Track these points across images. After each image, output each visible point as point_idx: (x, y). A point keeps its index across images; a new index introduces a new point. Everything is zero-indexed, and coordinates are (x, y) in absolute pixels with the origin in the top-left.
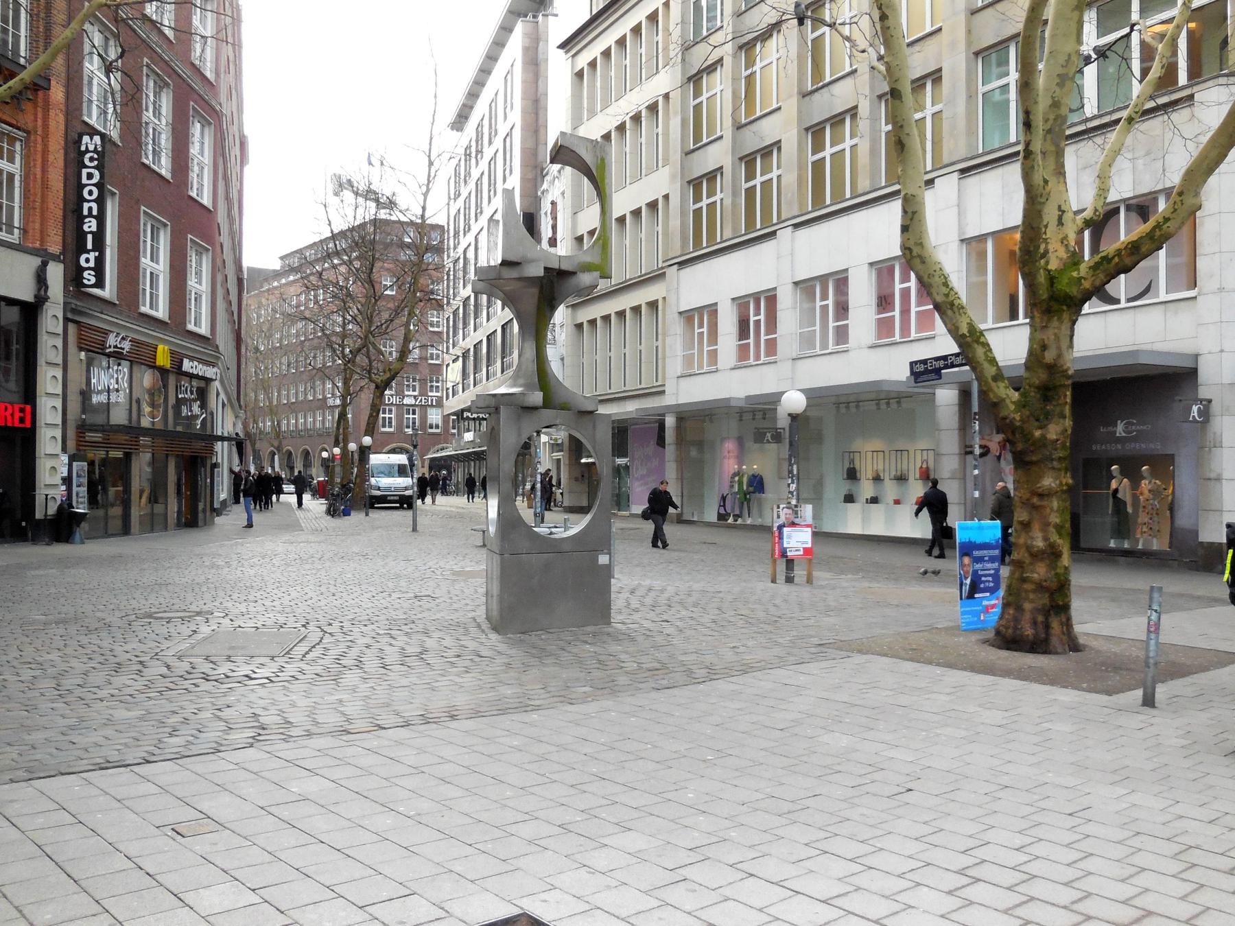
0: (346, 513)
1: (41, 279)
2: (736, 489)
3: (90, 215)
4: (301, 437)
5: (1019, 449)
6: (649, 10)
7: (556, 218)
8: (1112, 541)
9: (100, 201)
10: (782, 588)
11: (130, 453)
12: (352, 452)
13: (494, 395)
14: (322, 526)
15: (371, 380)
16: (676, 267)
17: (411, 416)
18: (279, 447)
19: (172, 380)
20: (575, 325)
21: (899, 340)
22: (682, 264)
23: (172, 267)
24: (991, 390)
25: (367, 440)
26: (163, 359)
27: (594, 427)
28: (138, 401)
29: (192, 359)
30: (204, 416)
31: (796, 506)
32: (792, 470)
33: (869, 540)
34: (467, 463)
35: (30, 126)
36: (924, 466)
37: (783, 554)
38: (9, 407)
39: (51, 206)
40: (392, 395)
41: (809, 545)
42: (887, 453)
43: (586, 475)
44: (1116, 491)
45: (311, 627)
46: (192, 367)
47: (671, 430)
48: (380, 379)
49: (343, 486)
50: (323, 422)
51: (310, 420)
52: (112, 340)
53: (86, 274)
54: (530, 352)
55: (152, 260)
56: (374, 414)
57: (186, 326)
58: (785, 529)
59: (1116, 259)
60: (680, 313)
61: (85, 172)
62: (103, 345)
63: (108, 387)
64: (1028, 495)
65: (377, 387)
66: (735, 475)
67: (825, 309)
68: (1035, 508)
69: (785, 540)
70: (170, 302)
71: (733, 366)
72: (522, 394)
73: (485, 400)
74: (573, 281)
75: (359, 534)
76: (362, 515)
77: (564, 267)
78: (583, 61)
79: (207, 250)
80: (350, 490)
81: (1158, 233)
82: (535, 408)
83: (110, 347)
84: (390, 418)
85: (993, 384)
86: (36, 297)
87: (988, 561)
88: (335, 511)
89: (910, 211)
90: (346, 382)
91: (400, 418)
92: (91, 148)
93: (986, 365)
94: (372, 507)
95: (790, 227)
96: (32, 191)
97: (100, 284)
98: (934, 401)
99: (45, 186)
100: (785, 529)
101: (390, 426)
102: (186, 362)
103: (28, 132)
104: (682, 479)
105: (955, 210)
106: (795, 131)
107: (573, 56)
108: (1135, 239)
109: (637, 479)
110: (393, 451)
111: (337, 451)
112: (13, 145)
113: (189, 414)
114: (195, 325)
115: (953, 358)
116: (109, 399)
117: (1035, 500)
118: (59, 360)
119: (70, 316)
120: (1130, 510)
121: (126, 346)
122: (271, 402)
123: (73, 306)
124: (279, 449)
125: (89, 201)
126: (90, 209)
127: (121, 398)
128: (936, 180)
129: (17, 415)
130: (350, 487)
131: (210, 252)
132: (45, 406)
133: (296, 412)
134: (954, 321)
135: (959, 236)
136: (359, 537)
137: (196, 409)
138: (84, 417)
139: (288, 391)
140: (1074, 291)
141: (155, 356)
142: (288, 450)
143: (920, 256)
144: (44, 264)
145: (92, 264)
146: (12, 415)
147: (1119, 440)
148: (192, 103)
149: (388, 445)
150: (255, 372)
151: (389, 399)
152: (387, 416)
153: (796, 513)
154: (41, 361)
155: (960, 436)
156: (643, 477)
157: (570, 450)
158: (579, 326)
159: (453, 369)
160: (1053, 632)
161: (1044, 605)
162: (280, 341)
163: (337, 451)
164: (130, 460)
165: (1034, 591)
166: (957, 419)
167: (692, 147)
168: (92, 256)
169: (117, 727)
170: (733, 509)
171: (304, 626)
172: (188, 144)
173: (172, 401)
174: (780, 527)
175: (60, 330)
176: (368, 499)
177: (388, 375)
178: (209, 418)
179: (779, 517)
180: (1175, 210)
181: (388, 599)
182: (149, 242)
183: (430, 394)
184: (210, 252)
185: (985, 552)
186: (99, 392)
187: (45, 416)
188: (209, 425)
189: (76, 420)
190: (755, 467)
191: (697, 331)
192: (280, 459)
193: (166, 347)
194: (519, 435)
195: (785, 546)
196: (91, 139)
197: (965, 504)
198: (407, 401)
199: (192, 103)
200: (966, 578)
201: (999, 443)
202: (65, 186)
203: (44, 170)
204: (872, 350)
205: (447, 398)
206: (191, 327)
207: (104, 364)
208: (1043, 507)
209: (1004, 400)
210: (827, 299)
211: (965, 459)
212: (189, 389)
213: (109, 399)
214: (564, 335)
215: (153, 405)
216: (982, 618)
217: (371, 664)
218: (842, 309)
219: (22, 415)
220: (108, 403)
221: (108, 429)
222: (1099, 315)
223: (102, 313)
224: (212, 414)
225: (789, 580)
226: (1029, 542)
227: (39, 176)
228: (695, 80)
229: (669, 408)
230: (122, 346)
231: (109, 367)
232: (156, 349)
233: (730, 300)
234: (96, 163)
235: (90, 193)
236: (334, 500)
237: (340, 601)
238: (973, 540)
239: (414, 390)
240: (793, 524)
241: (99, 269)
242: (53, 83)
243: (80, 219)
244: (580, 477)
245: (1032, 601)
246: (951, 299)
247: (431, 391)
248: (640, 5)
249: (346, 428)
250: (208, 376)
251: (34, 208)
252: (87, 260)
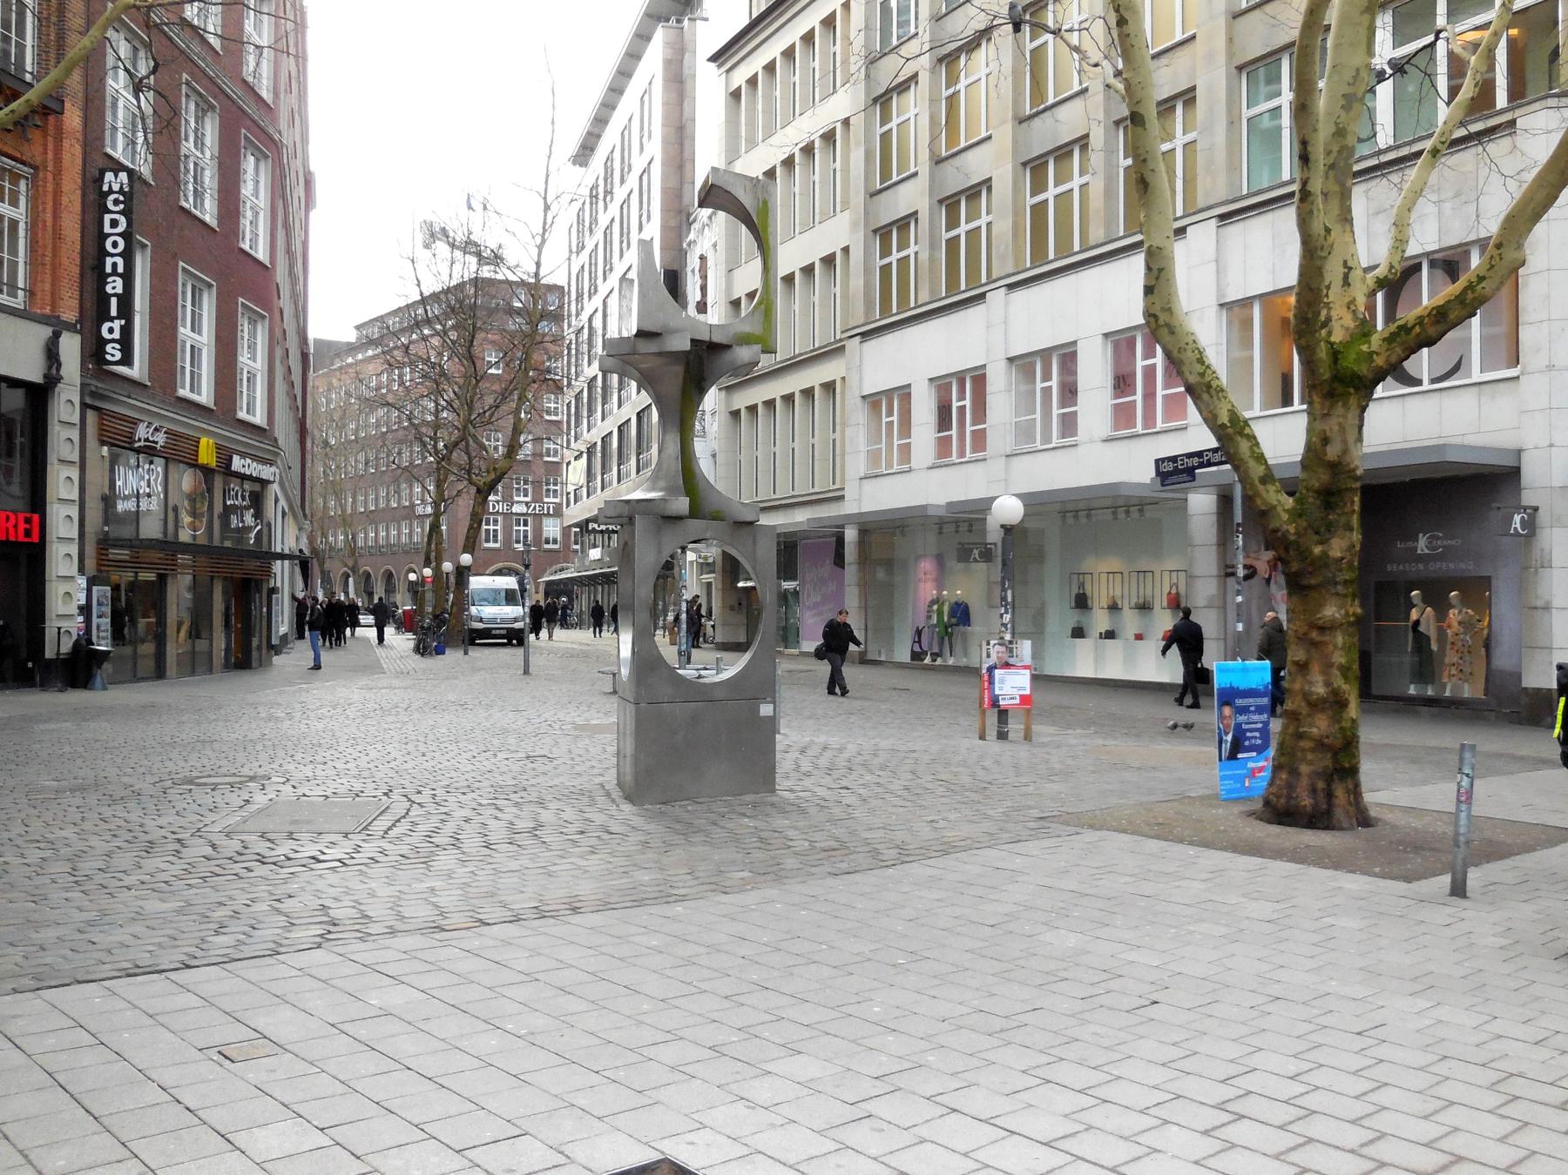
0: (440, 651)
1: (52, 354)
2: (934, 620)
3: (114, 273)
4: (383, 554)
5: (1293, 570)
6: (825, 13)
7: (706, 277)
8: (1412, 686)
9: (128, 255)
10: (993, 746)
11: (165, 575)
12: (447, 574)
13: (628, 502)
14: (409, 667)
15: (471, 482)
16: (858, 339)
17: (522, 528)
18: (354, 567)
19: (218, 482)
20: (730, 413)
21: (1141, 432)
22: (865, 335)
23: (218, 338)
24: (1258, 494)
25: (466, 559)
26: (207, 456)
27: (754, 542)
28: (175, 509)
29: (243, 455)
30: (259, 527)
31: (1011, 642)
32: (1006, 597)
33: (1103, 685)
34: (592, 588)
35: (38, 160)
36: (1174, 591)
37: (995, 702)
38: (12, 516)
39: (65, 261)
40: (498, 502)
41: (1028, 692)
42: (1126, 575)
43: (744, 603)
44: (1417, 623)
45: (395, 796)
46: (244, 466)
47: (852, 546)
48: (483, 480)
49: (436, 617)
50: (410, 535)
51: (394, 533)
52: (142, 432)
53: (109, 348)
54: (673, 447)
55: (193, 330)
56: (475, 526)
57: (236, 414)
58: (997, 672)
59: (1417, 329)
60: (864, 397)
61: (107, 218)
62: (131, 438)
63: (138, 491)
64: (1305, 629)
65: (479, 491)
66: (933, 602)
67: (1047, 392)
68: (1315, 644)
69: (997, 685)
70: (216, 383)
71: (930, 464)
72: (663, 500)
73: (615, 507)
74: (727, 357)
75: (456, 678)
76: (459, 654)
77: (717, 339)
78: (740, 77)
79: (263, 317)
80: (444, 622)
81: (1470, 296)
82: (679, 518)
83: (140, 440)
84: (495, 531)
85: (1261, 487)
86: (45, 376)
87: (1254, 712)
88: (425, 648)
89: (1155, 267)
90: (439, 485)
91: (507, 530)
92: (116, 187)
93: (1252, 463)
94: (473, 643)
95: (1003, 289)
96: (40, 243)
97: (127, 360)
98: (1186, 508)
99: (57, 235)
100: (997, 672)
101: (496, 541)
102: (236, 459)
103: (35, 168)
104: (866, 608)
105: (1213, 266)
106: (1010, 166)
107: (728, 71)
108: (1441, 303)
109: (809, 608)
110: (499, 573)
111: (428, 572)
112: (17, 184)
113: (240, 525)
114: (248, 412)
115: (1210, 454)
116: (138, 506)
117: (1314, 635)
118: (75, 457)
119: (88, 400)
120: (1434, 647)
121: (161, 439)
122: (344, 511)
123: (93, 389)
124: (354, 569)
125: (113, 255)
126: (115, 265)
127: (153, 505)
128: (1188, 229)
129: (22, 526)
130: (445, 618)
131: (267, 320)
132: (57, 515)
133: (376, 523)
134: (1212, 407)
135: (1218, 300)
136: (455, 681)
137: (249, 518)
138: (106, 529)
139: (366, 496)
140: (1364, 370)
141: (197, 451)
142: (365, 571)
143: (1167, 325)
144: (56, 335)
145: (116, 335)
146: (15, 526)
147: (1421, 558)
148: (243, 131)
149: (493, 565)
150: (324, 472)
151: (494, 507)
152: (491, 527)
153: (1011, 651)
154: (52, 458)
155: (1219, 553)
156: (816, 605)
157: (724, 571)
158: (735, 414)
159: (575, 468)
160: (1337, 801)
161: (1326, 767)
162: (356, 432)
163: (428, 572)
164: (166, 584)
165: (1313, 750)
166: (1215, 532)
167: (878, 187)
168: (117, 325)
169: (148, 923)
170: (931, 646)
171: (385, 794)
173: (218, 508)
174: (991, 669)
175: (76, 419)
176: (467, 633)
177: (493, 476)
178: (265, 531)
179: (988, 656)
180: (1492, 267)
181: (493, 760)
182: (189, 308)
183: (546, 500)
184: (267, 320)
185: (1251, 700)
186: (126, 498)
187: (57, 528)
188: (265, 539)
189: (96, 533)
190: (959, 592)
191: (885, 420)
192: (356, 583)
193: (211, 441)
194: (660, 552)
195: (997, 693)
196: (116, 177)
197: (1225, 639)
198: (516, 509)
199: (243, 131)
200: (1227, 734)
201: (1269, 562)
202: (83, 236)
203: (56, 216)
204: (1107, 444)
205: (568, 505)
206: (242, 415)
207: (133, 461)
208: (1324, 643)
209: (1274, 507)
210: (1050, 379)
211: (1225, 583)
212: (239, 494)
213: (138, 506)
214: (716, 425)
215: (194, 514)
216: (1247, 784)
217: (471, 843)
218: (1070, 392)
219: (28, 526)
220: (138, 512)
221: (137, 545)
222: (1395, 400)
223: (129, 397)
224: (269, 525)
225: (1002, 736)
226: (1307, 688)
227: (49, 223)
228: (882, 101)
229: (849, 518)
230: (155, 439)
231: (138, 466)
232: (198, 442)
233: (927, 381)
234: (122, 206)
235: (115, 245)
236: (424, 634)
237: (431, 763)
238: (1235, 685)
239: (526, 495)
240: (1007, 665)
241: (126, 342)
242: (67, 105)
243: (102, 278)
244: (737, 605)
245: (1310, 763)
246: (1208, 379)
247: (548, 496)
248: (812, 6)
249: (439, 543)
250: (264, 478)
251: (44, 265)
252: (111, 330)
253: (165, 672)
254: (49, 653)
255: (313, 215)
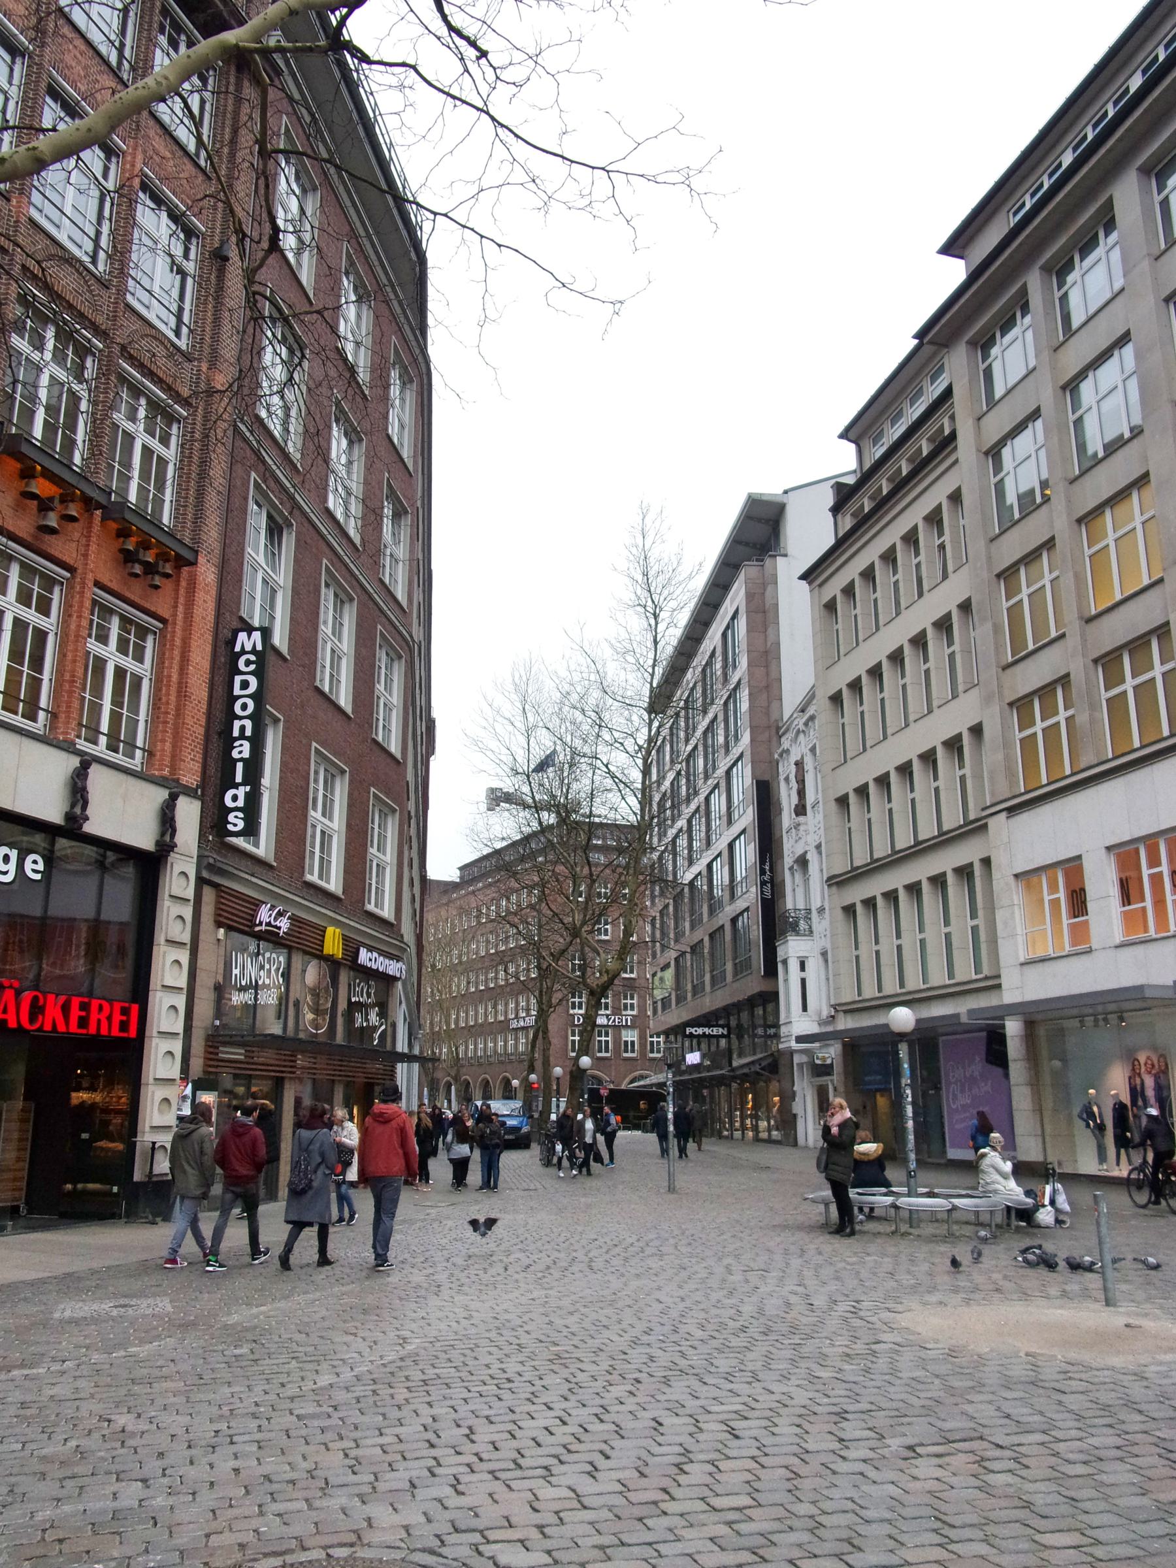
1: (167, 820)
3: (242, 736)
4: (480, 1065)
7: (803, 781)
9: (256, 717)
11: (283, 1079)
12: (558, 1079)
16: (1004, 815)
19: (344, 977)
21: (1154, 936)
22: (1012, 811)
23: (349, 826)
26: (333, 944)
28: (297, 1004)
29: (371, 949)
30: (383, 1027)
35: (166, 614)
38: (106, 1005)
39: (189, 720)
47: (1017, 1040)
50: (516, 1045)
51: (501, 1043)
52: (264, 915)
53: (231, 817)
55: (324, 815)
60: (1016, 876)
61: (238, 679)
62: (251, 921)
63: (256, 982)
67: (1055, 903)
70: (345, 872)
78: (834, 588)
79: (394, 811)
83: (261, 923)
86: (158, 843)
92: (248, 648)
96: (164, 699)
97: (251, 830)
99: (183, 692)
103: (163, 621)
107: (820, 585)
112: (144, 640)
114: (376, 906)
116: (256, 999)
118: (186, 937)
119: (205, 874)
121: (284, 924)
122: (448, 1024)
123: (211, 861)
124: (456, 1078)
125: (241, 718)
126: (243, 728)
127: (269, 998)
129: (118, 1018)
131: (398, 814)
132: (160, 1005)
137: (373, 1018)
138: (217, 1023)
144: (173, 798)
145: (240, 803)
146: (109, 1018)
148: (379, 627)
154: (160, 938)
162: (460, 956)
164: (283, 1088)
167: (1010, 659)
168: (241, 792)
172: (411, 229)
173: (342, 1005)
175: (190, 893)
177: (605, 978)
182: (321, 792)
184: (398, 814)
186: (243, 989)
187: (159, 1019)
188: (389, 1039)
189: (206, 1029)
191: (1047, 898)
192: (457, 1090)
196: (249, 636)
199: (379, 627)
202: (211, 697)
203: (183, 671)
206: (371, 907)
207: (252, 948)
210: (1159, 864)
213: (256, 999)
215: (316, 1011)
218: (1078, 902)
220: (255, 1005)
221: (256, 1041)
223: (252, 875)
227: (175, 677)
230: (278, 923)
231: (258, 954)
232: (325, 932)
233: (1104, 850)
234: (253, 667)
235: (244, 707)
241: (251, 810)
242: (201, 560)
243: (228, 742)
244: (861, 1108)
249: (545, 1051)
251: (166, 722)
252: (235, 798)
253: (277, 1193)
254: (137, 1176)
255: (434, 763)
